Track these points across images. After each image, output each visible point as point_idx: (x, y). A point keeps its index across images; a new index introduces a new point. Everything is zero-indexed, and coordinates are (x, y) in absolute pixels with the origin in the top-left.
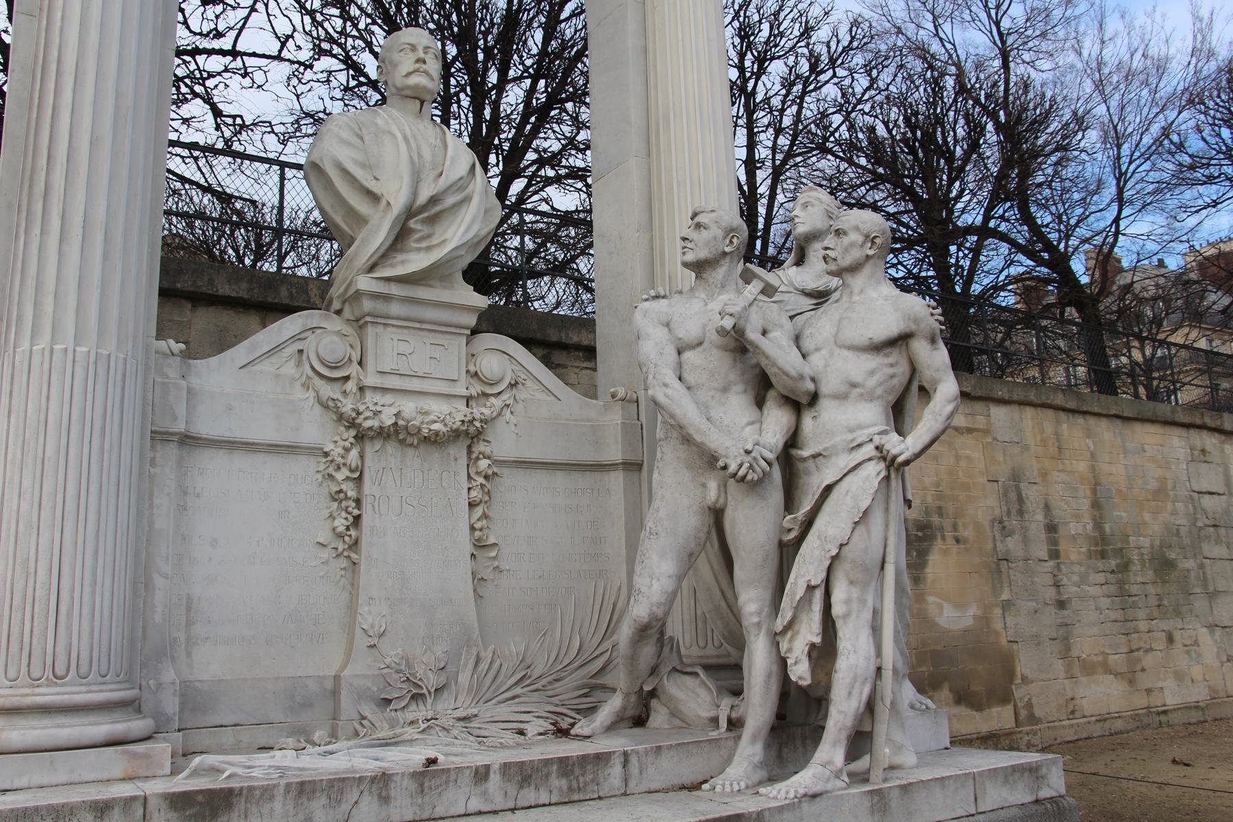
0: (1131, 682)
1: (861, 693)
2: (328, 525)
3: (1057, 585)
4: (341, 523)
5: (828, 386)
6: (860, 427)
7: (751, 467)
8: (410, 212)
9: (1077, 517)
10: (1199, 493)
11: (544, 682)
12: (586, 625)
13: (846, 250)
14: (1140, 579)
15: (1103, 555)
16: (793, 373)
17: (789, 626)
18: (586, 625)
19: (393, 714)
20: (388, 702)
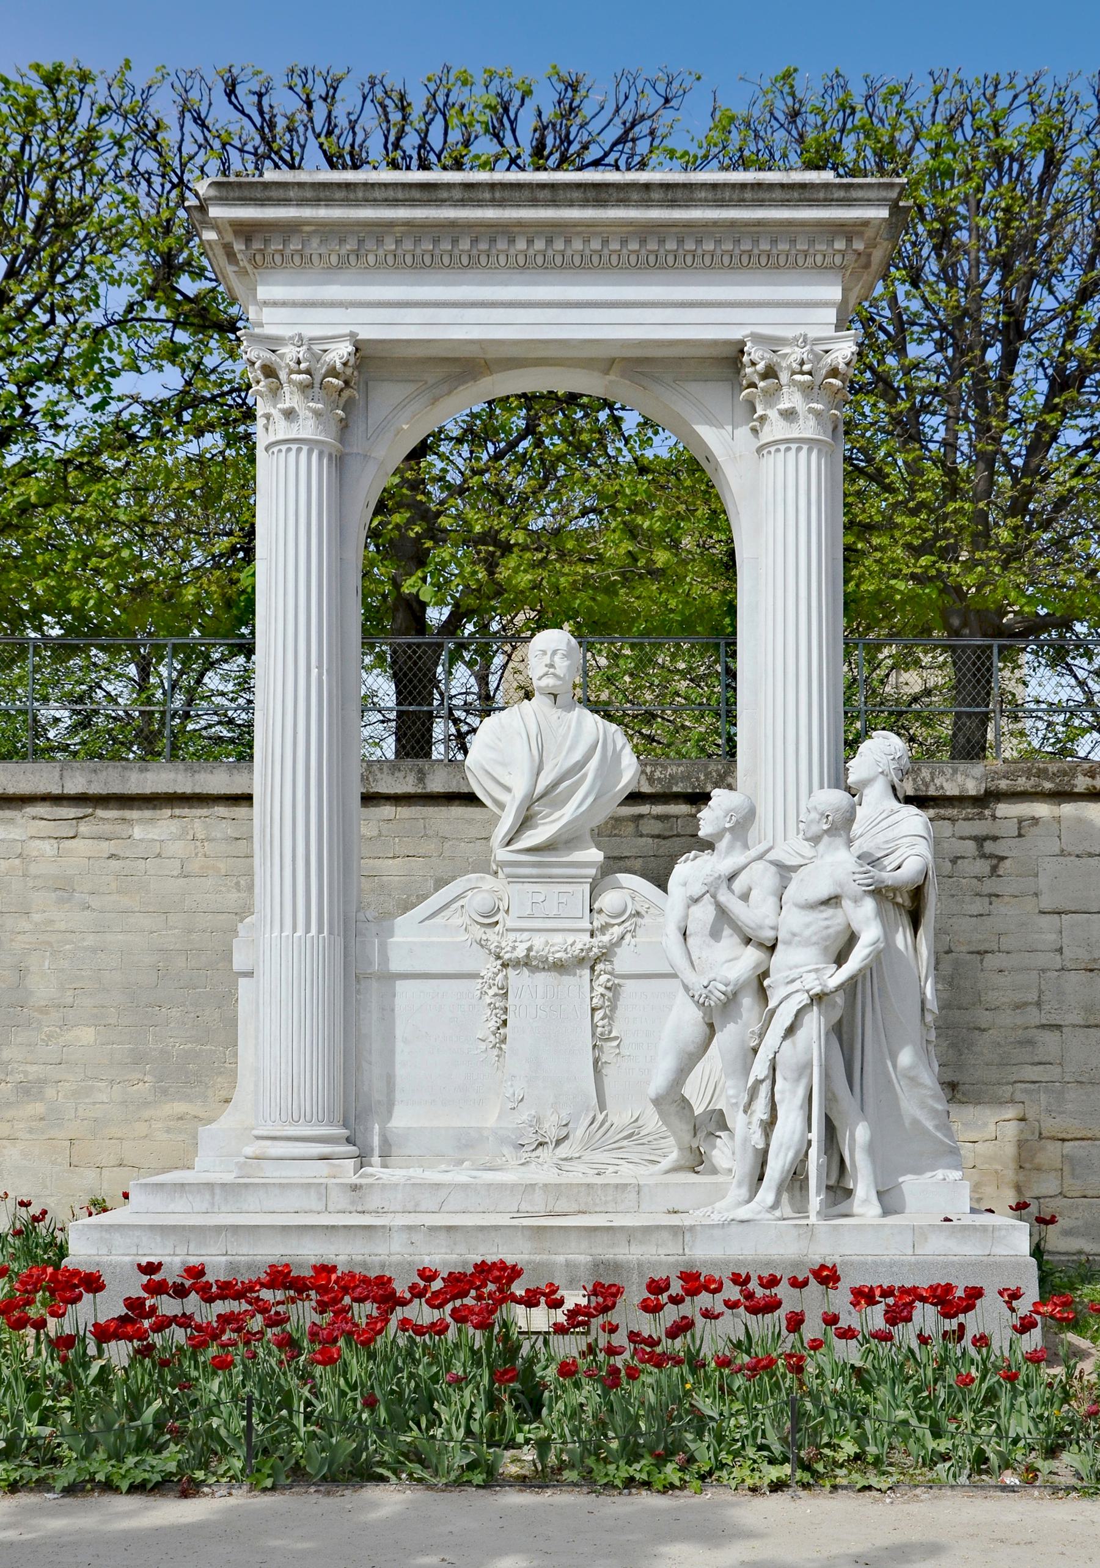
4: (493, 1024)
6: (796, 967)
11: (650, 1138)
16: (752, 925)
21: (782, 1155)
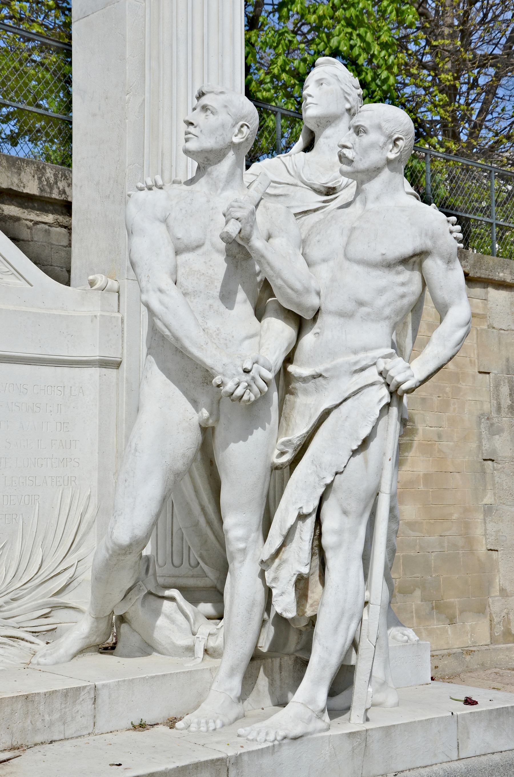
1: (348, 628)
6: (365, 349)
12: (50, 536)
13: (365, 151)
16: (298, 286)
18: (50, 536)
21: (343, 627)
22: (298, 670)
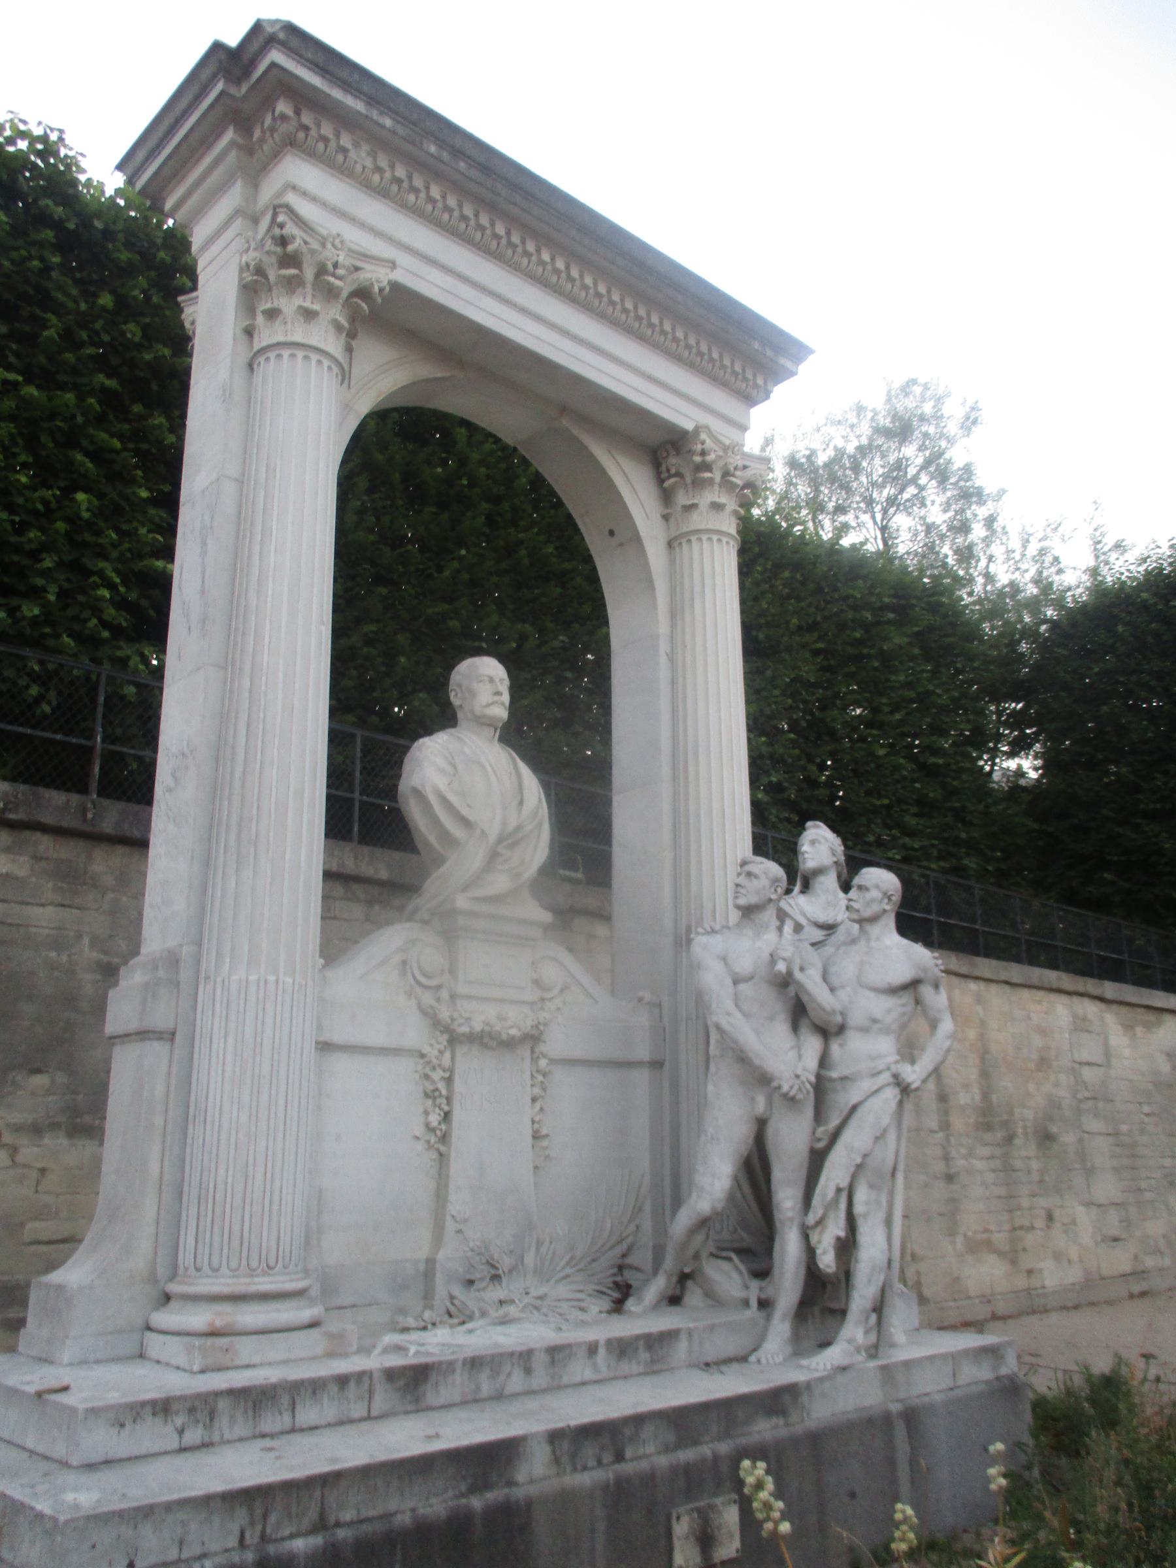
0: (1013, 1262)
2: (421, 1120)
3: (946, 1158)
4: (434, 1119)
5: (856, 1018)
7: (800, 1089)
8: (500, 840)
9: (966, 1086)
10: (1080, 1063)
14: (1023, 1153)
15: (988, 1127)
16: (828, 1008)
17: (820, 1222)
19: (477, 1294)
20: (471, 1282)
22: (814, 564)
